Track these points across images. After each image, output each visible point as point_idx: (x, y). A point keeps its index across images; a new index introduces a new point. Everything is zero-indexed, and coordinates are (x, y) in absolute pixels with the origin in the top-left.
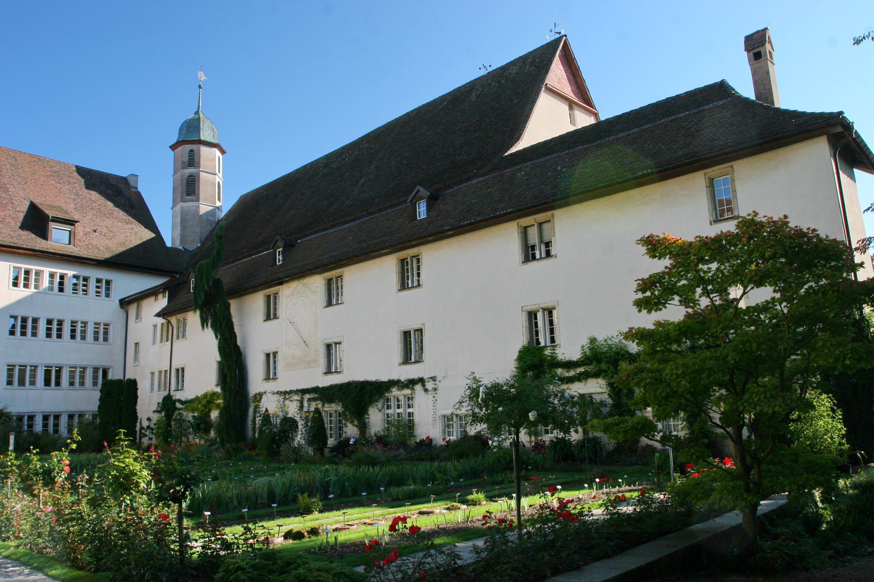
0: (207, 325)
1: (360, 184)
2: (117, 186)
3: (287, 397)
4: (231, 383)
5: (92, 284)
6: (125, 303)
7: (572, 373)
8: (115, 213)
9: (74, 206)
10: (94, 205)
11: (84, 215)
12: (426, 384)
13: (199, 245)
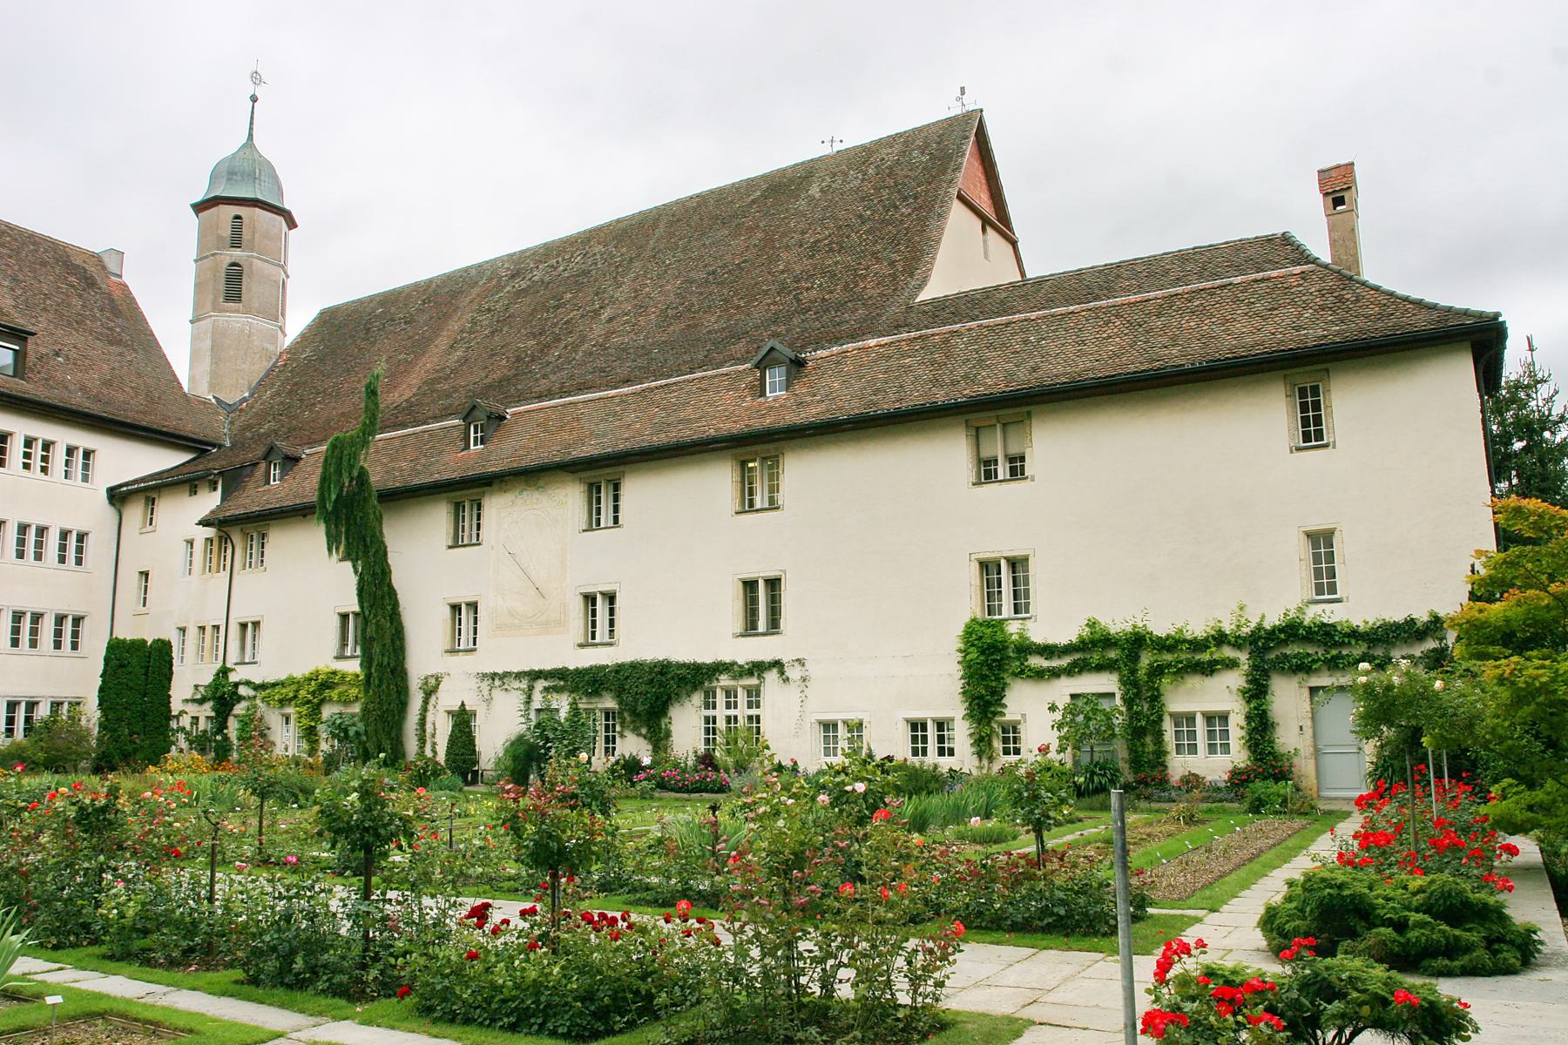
0: (337, 549)
1: (605, 316)
2: (84, 268)
3: (497, 683)
4: (383, 655)
5: (59, 456)
6: (118, 497)
7: (1055, 663)
8: (88, 322)
9: (13, 303)
10: (48, 302)
11: (33, 321)
12: (786, 669)
13: (247, 394)
